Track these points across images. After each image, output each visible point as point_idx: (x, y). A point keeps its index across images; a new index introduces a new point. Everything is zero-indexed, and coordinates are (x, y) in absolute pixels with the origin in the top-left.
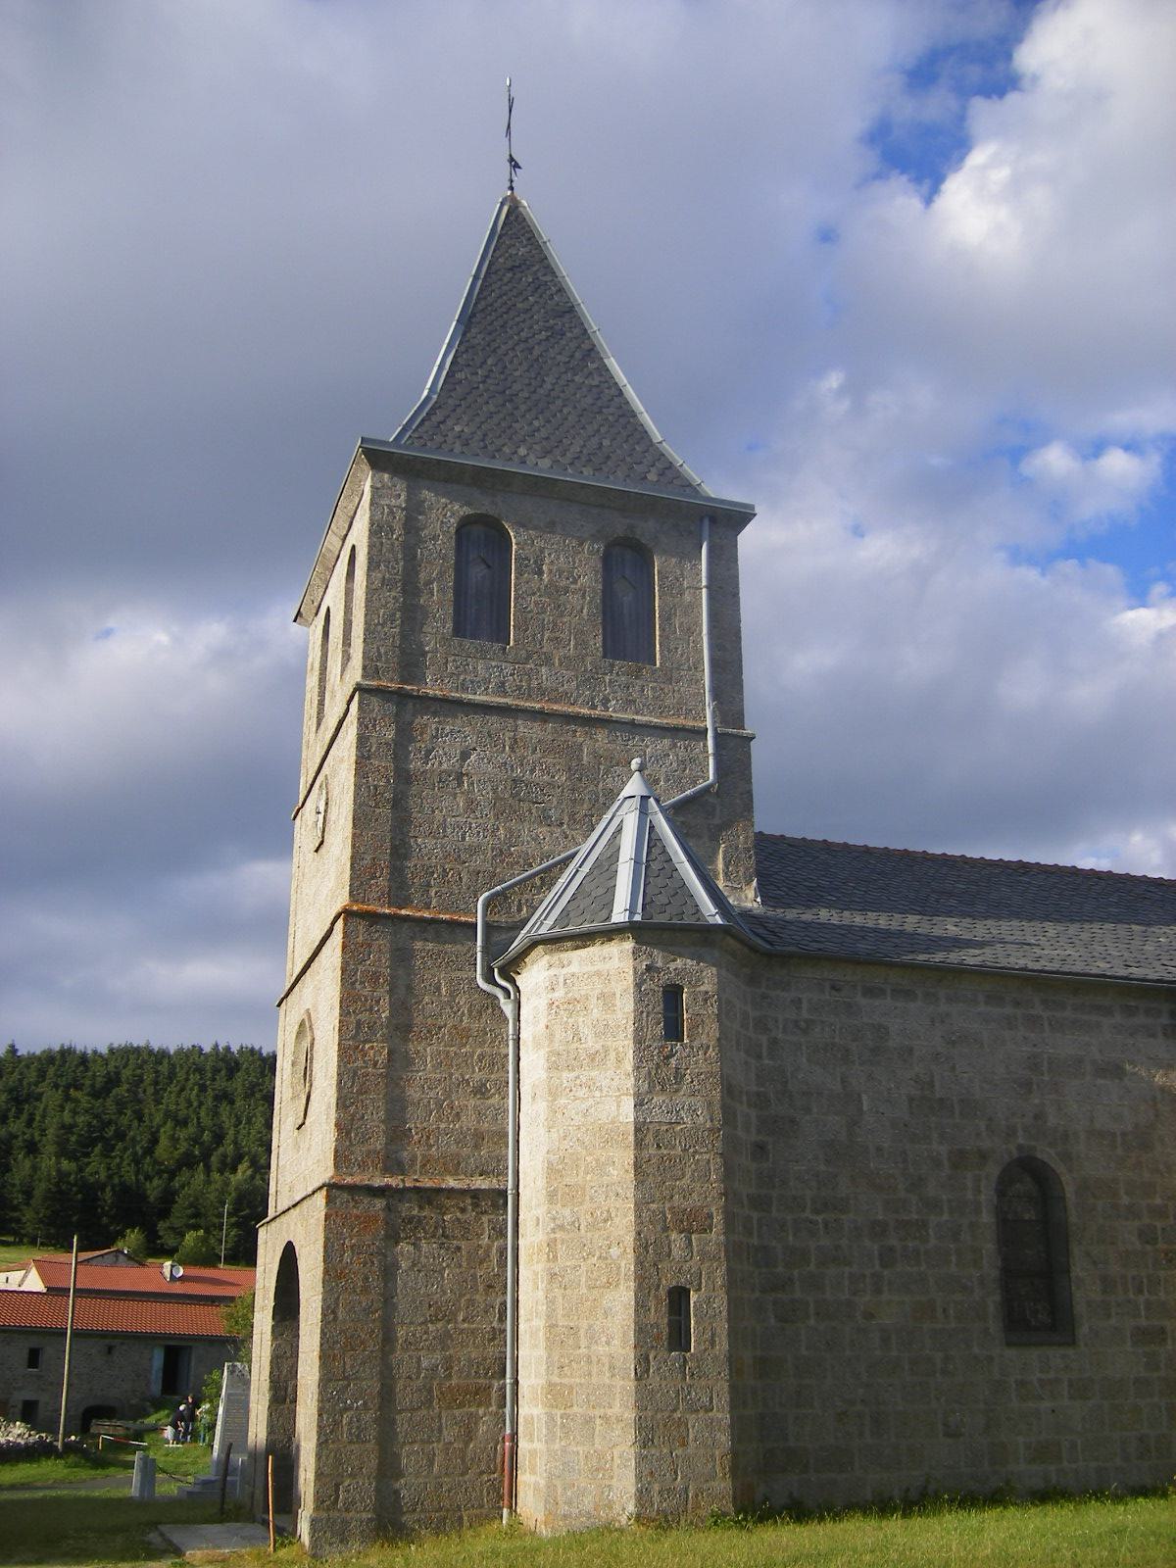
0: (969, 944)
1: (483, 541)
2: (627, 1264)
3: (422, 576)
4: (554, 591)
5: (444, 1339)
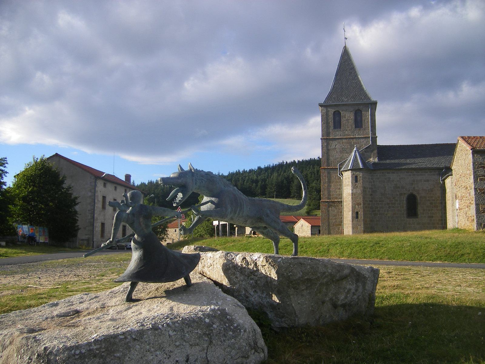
0: (411, 164)
1: (337, 114)
2: (351, 209)
3: (329, 121)
4: (347, 120)
5: (336, 219)
